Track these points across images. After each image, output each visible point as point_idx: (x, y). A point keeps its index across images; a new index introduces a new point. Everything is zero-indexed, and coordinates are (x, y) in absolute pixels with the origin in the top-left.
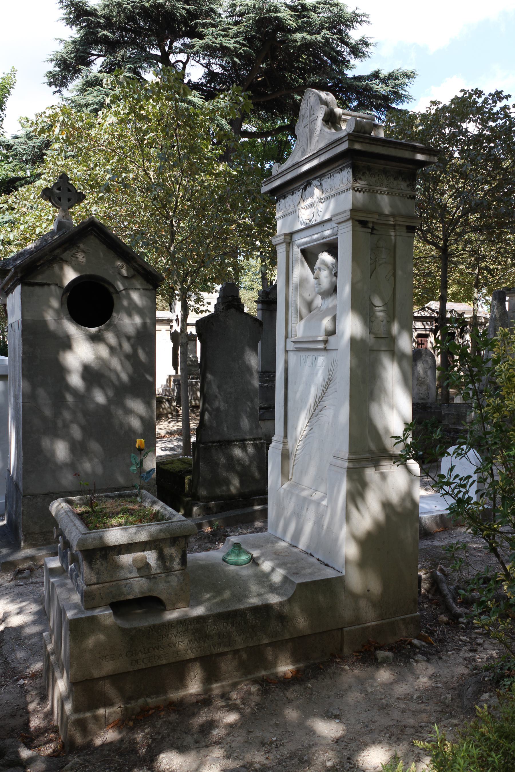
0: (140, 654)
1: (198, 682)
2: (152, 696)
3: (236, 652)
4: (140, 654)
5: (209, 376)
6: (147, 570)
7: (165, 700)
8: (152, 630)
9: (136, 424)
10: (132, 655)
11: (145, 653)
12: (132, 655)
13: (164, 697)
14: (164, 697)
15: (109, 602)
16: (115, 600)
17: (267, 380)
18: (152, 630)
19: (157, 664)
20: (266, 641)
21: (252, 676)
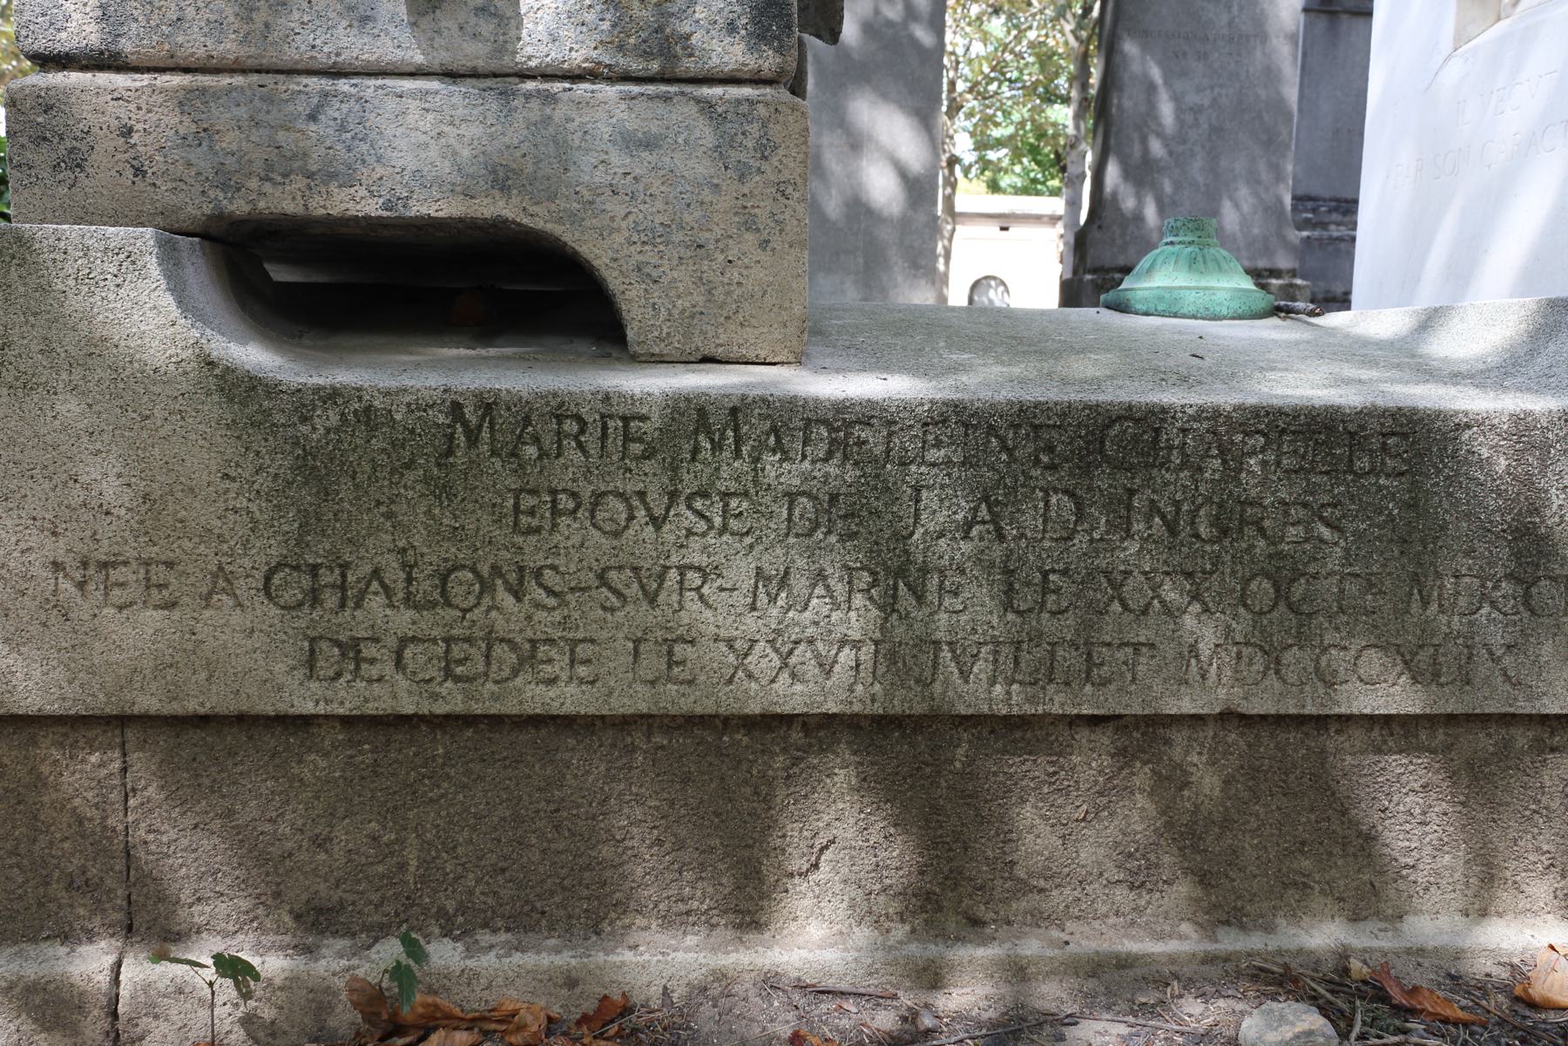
0: (376, 603)
1: (837, 908)
2: (485, 937)
3: (1140, 735)
4: (376, 603)
5: (1130, 47)
6: (486, 27)
7: (571, 983)
8: (473, 437)
9: (882, 187)
10: (314, 597)
11: (408, 600)
12: (314, 597)
13: (566, 959)
14: (566, 959)
15: (196, 208)
16: (238, 206)
17: (1307, 221)
18: (473, 437)
19: (510, 707)
20: (1395, 696)
21: (1255, 942)
